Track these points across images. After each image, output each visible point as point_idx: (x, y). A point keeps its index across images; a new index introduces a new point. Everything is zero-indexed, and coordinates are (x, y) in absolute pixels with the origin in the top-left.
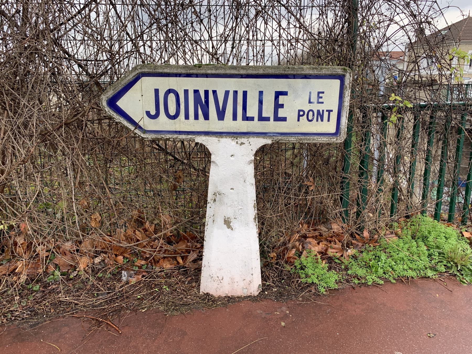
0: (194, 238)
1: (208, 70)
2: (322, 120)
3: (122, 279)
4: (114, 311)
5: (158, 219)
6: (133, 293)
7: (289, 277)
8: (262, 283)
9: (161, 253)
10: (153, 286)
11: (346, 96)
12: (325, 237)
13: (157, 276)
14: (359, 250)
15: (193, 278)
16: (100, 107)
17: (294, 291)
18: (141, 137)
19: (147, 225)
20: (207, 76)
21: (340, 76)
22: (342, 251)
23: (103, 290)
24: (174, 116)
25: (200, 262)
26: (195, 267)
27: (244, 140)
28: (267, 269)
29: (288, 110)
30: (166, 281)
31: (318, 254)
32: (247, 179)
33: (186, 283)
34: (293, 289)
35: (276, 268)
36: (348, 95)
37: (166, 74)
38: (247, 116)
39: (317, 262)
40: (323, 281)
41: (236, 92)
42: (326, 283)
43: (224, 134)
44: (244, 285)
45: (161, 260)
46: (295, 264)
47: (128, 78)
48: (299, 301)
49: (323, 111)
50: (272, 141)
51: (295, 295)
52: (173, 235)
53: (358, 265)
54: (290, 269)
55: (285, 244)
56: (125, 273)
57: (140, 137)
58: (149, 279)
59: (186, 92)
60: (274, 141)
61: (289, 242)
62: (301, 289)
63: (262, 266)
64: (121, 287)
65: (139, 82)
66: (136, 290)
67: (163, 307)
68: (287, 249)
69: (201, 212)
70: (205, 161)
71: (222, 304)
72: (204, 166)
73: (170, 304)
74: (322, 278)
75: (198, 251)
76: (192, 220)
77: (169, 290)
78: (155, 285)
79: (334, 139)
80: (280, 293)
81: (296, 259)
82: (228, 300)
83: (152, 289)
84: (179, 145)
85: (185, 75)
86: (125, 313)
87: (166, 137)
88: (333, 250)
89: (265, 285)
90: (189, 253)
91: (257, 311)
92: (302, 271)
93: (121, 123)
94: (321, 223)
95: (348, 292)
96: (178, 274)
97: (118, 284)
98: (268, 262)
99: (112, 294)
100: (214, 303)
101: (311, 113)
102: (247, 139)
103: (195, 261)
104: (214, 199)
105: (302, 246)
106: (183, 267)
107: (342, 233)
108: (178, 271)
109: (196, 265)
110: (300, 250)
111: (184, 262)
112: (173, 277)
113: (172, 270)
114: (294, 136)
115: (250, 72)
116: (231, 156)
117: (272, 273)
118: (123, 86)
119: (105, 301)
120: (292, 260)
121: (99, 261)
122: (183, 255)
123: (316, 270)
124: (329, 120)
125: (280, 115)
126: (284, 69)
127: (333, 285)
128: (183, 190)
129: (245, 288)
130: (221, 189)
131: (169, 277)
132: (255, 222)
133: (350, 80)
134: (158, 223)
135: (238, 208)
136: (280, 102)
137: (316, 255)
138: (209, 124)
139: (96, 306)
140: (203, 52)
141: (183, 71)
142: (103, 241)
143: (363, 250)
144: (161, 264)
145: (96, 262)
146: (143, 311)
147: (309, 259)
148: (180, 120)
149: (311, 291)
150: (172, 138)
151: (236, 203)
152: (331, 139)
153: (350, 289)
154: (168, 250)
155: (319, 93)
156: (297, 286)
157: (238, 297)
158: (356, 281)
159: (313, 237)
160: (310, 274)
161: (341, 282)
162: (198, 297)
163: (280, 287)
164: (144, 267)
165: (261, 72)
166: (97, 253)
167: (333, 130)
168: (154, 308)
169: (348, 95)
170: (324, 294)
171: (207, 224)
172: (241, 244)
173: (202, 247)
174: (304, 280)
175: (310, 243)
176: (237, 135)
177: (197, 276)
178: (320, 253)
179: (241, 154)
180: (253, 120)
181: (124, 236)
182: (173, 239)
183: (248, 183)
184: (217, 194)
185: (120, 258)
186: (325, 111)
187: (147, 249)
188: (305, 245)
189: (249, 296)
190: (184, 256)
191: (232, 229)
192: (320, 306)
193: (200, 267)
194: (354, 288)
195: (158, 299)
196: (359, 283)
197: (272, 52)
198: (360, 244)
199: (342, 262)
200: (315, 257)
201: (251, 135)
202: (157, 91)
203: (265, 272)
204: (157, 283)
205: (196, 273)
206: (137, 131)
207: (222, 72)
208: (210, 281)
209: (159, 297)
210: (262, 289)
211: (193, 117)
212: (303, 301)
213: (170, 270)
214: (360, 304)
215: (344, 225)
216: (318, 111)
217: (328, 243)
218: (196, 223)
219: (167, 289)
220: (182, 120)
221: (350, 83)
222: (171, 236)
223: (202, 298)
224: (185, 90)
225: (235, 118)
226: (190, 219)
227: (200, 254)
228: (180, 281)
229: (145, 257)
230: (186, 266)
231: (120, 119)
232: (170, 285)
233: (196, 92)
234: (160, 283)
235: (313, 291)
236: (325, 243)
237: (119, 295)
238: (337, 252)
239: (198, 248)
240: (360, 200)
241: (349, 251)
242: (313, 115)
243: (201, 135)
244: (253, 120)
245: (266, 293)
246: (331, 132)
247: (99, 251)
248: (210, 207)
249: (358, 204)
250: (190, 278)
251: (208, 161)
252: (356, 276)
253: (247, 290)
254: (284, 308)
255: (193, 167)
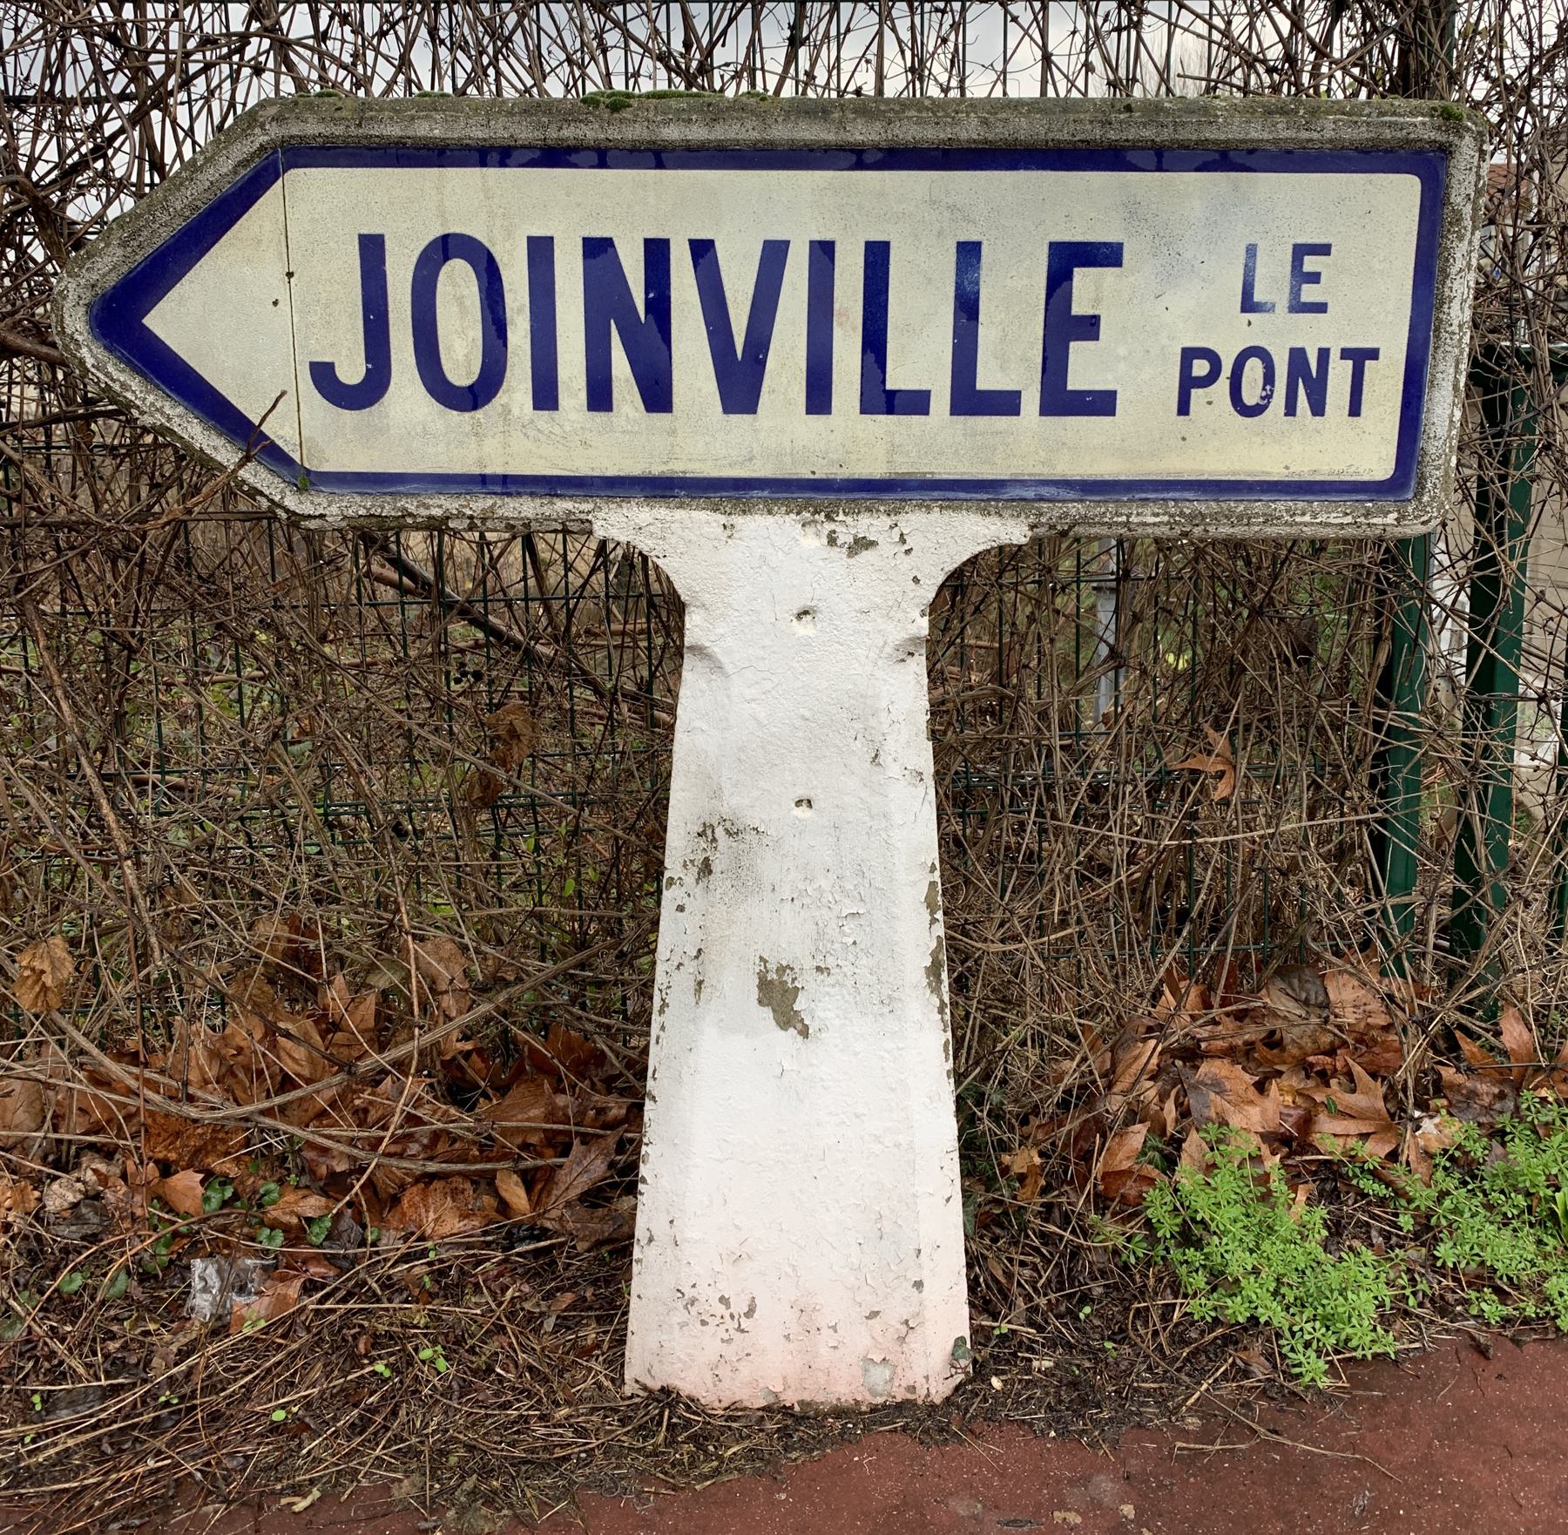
0: (588, 1062)
1: (666, 123)
2: (1318, 409)
3: (189, 1304)
4: (130, 1510)
5: (394, 966)
6: (248, 1388)
7: (1116, 1287)
8: (975, 1330)
9: (414, 1148)
10: (362, 1347)
11: (1454, 270)
12: (1295, 1051)
13: (387, 1284)
14: (1483, 1120)
15: (584, 1299)
16: (53, 345)
17: (1149, 1369)
18: (287, 511)
19: (336, 995)
20: (658, 156)
21: (1421, 152)
22: (1387, 1128)
23: (81, 1370)
24: (471, 388)
25: (627, 1201)
26: (593, 1233)
27: (871, 524)
28: (995, 1240)
29: (1122, 351)
30: (435, 1317)
31: (1265, 1150)
32: (890, 748)
33: (549, 1324)
34: (1147, 1356)
35: (1044, 1237)
36: (1469, 266)
37: (426, 147)
38: (889, 386)
39: (1266, 1197)
40: (1308, 1313)
41: (823, 252)
42: (1328, 1321)
43: (755, 493)
44: (868, 1342)
45: (411, 1196)
46: (1149, 1212)
47: (210, 174)
48: (1185, 1434)
49: (1324, 354)
50: (1032, 527)
51: (1162, 1399)
52: (479, 1051)
53: (1490, 1207)
54: (1121, 1241)
55: (1091, 1101)
56: (211, 1271)
57: (280, 512)
58: (344, 1300)
59: (541, 251)
60: (1041, 531)
61: (1109, 1086)
62: (1187, 1359)
63: (970, 1233)
64: (183, 1354)
65: (268, 203)
66: (269, 1370)
67: (416, 1477)
68: (1100, 1127)
69: (628, 925)
70: (649, 649)
71: (752, 1454)
72: (646, 674)
73: (453, 1460)
74: (1301, 1292)
75: (612, 1138)
76: (582, 966)
77: (452, 1370)
78: (377, 1341)
79: (1386, 514)
80: (1074, 1385)
81: (1151, 1181)
82: (784, 1432)
83: (355, 1361)
84: (513, 563)
85: (537, 154)
86: (192, 1519)
87: (424, 512)
88: (1341, 1126)
89: (988, 1339)
90: (565, 1151)
91: (952, 1503)
92: (1191, 1252)
93: (173, 433)
94: (1269, 972)
95: (1454, 1372)
96: (500, 1275)
97: (167, 1337)
98: (999, 1203)
99: (129, 1398)
100: (706, 1451)
101: (1254, 368)
102: (888, 521)
103: (595, 1197)
104: (700, 858)
105: (1178, 1105)
106: (532, 1228)
107: (1387, 1028)
108: (500, 1256)
109: (602, 1219)
110: (1170, 1129)
111: (538, 1203)
112: (477, 1289)
113: (469, 1246)
114: (1155, 501)
115: (910, 132)
116: (799, 616)
117: (1023, 1264)
118: (179, 224)
119: (86, 1444)
120: (1130, 1188)
121: (71, 1198)
122: (530, 1163)
123: (1265, 1246)
124: (1355, 410)
125: (1076, 382)
126: (1100, 116)
127: (1366, 1338)
128: (533, 806)
129: (878, 1359)
130: (739, 802)
131: (454, 1292)
132: (936, 990)
133: (1479, 177)
134: (394, 989)
135: (836, 908)
136: (1080, 306)
137: (1256, 1159)
138: (673, 432)
139: (33, 1476)
140: (637, 58)
141: (525, 133)
142: (90, 1090)
143: (1503, 1120)
144: (410, 1212)
145: (53, 1204)
146: (301, 1504)
147: (1225, 1182)
148: (507, 410)
149: (1246, 1374)
150: (460, 515)
151: (825, 883)
152: (1366, 516)
153: (1463, 1355)
154: (449, 1133)
155: (1300, 251)
156: (1162, 1339)
157: (839, 1412)
158: (1493, 1309)
159: (1230, 1053)
160: (1234, 1269)
161: (1407, 1314)
162: (615, 1410)
163: (1070, 1346)
164: (317, 1234)
165: (969, 131)
166: (62, 1160)
167: (1379, 463)
168: (365, 1483)
169: (1469, 266)
170: (1320, 1392)
171: (664, 1005)
172: (857, 1116)
173: (635, 1114)
174: (1201, 1307)
175: (1218, 1086)
176: (832, 497)
177: (607, 1283)
178: (1277, 1140)
179: (858, 605)
180: (925, 411)
181: (214, 1055)
182: (475, 1070)
183: (894, 770)
184: (720, 832)
185: (187, 1182)
186: (1335, 356)
187: (334, 1132)
188: (1192, 1101)
189: (901, 1407)
190: (537, 1169)
191: (804, 1032)
192: (1310, 1465)
193: (626, 1229)
194: (1482, 1351)
195: (387, 1429)
196: (1507, 1321)
197: (1006, 62)
198: (1486, 1089)
199: (1399, 1193)
200: (1248, 1169)
201: (908, 495)
202: (372, 249)
203: (985, 1258)
204: (382, 1328)
205: (602, 1262)
206: (255, 475)
207: (743, 135)
208: (683, 1325)
209: (394, 1413)
210: (975, 1362)
211: (583, 396)
212: (1206, 1435)
213: (458, 1245)
214: (1534, 1456)
215: (1396, 986)
216: (1298, 356)
217: (1311, 1083)
218: (600, 984)
219: (442, 1364)
220: (516, 411)
221: (1478, 192)
222: (467, 1055)
223: (636, 1423)
224: (530, 240)
225: (819, 398)
226: (571, 960)
227: (621, 1158)
228: (511, 1316)
229: (323, 1170)
230: (548, 1225)
231: (168, 411)
232: (459, 1341)
233: (598, 250)
234: (403, 1325)
235: (1260, 1370)
236: (1293, 1081)
237: (167, 1404)
238: (1364, 1137)
239: (608, 1126)
240: (1482, 851)
241: (1428, 1125)
242: (1269, 378)
243: (626, 498)
244: (925, 411)
245: (996, 1382)
246: (1366, 478)
247: (70, 1142)
248: (681, 909)
249: (1465, 868)
250: (568, 1298)
251: (665, 647)
252: (1485, 1278)
253: (887, 1373)
254: (1105, 1486)
255: (585, 681)
